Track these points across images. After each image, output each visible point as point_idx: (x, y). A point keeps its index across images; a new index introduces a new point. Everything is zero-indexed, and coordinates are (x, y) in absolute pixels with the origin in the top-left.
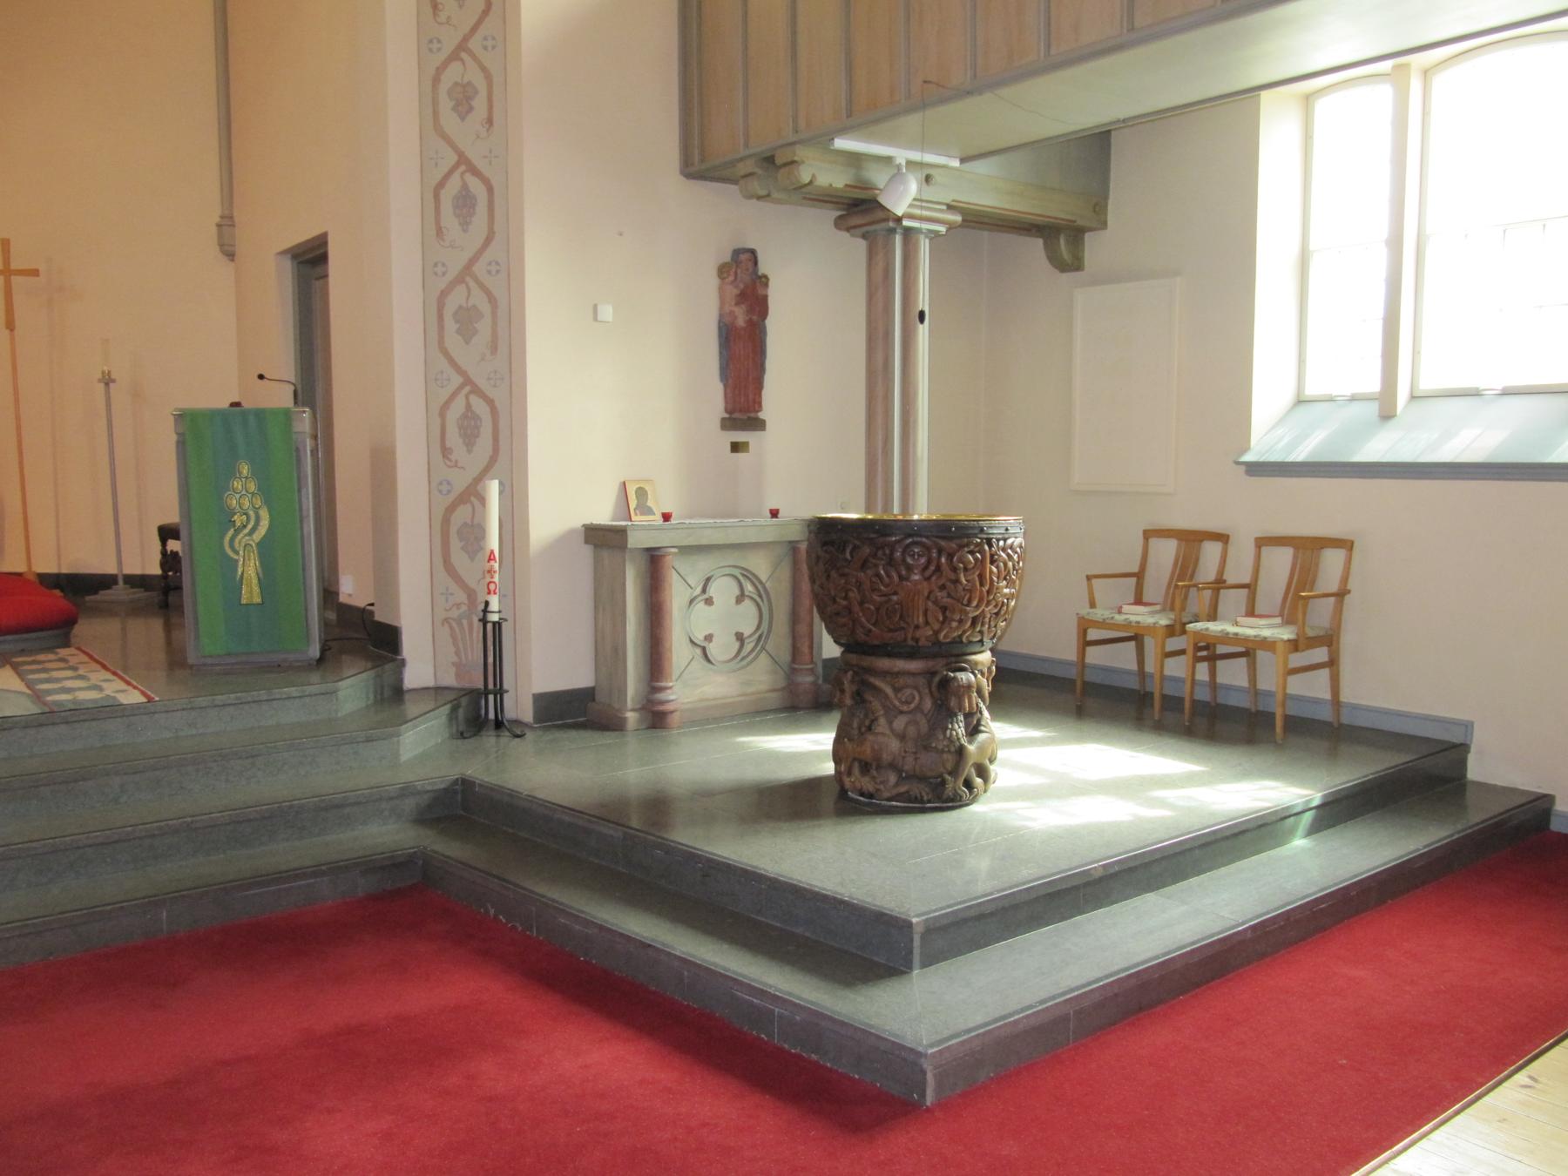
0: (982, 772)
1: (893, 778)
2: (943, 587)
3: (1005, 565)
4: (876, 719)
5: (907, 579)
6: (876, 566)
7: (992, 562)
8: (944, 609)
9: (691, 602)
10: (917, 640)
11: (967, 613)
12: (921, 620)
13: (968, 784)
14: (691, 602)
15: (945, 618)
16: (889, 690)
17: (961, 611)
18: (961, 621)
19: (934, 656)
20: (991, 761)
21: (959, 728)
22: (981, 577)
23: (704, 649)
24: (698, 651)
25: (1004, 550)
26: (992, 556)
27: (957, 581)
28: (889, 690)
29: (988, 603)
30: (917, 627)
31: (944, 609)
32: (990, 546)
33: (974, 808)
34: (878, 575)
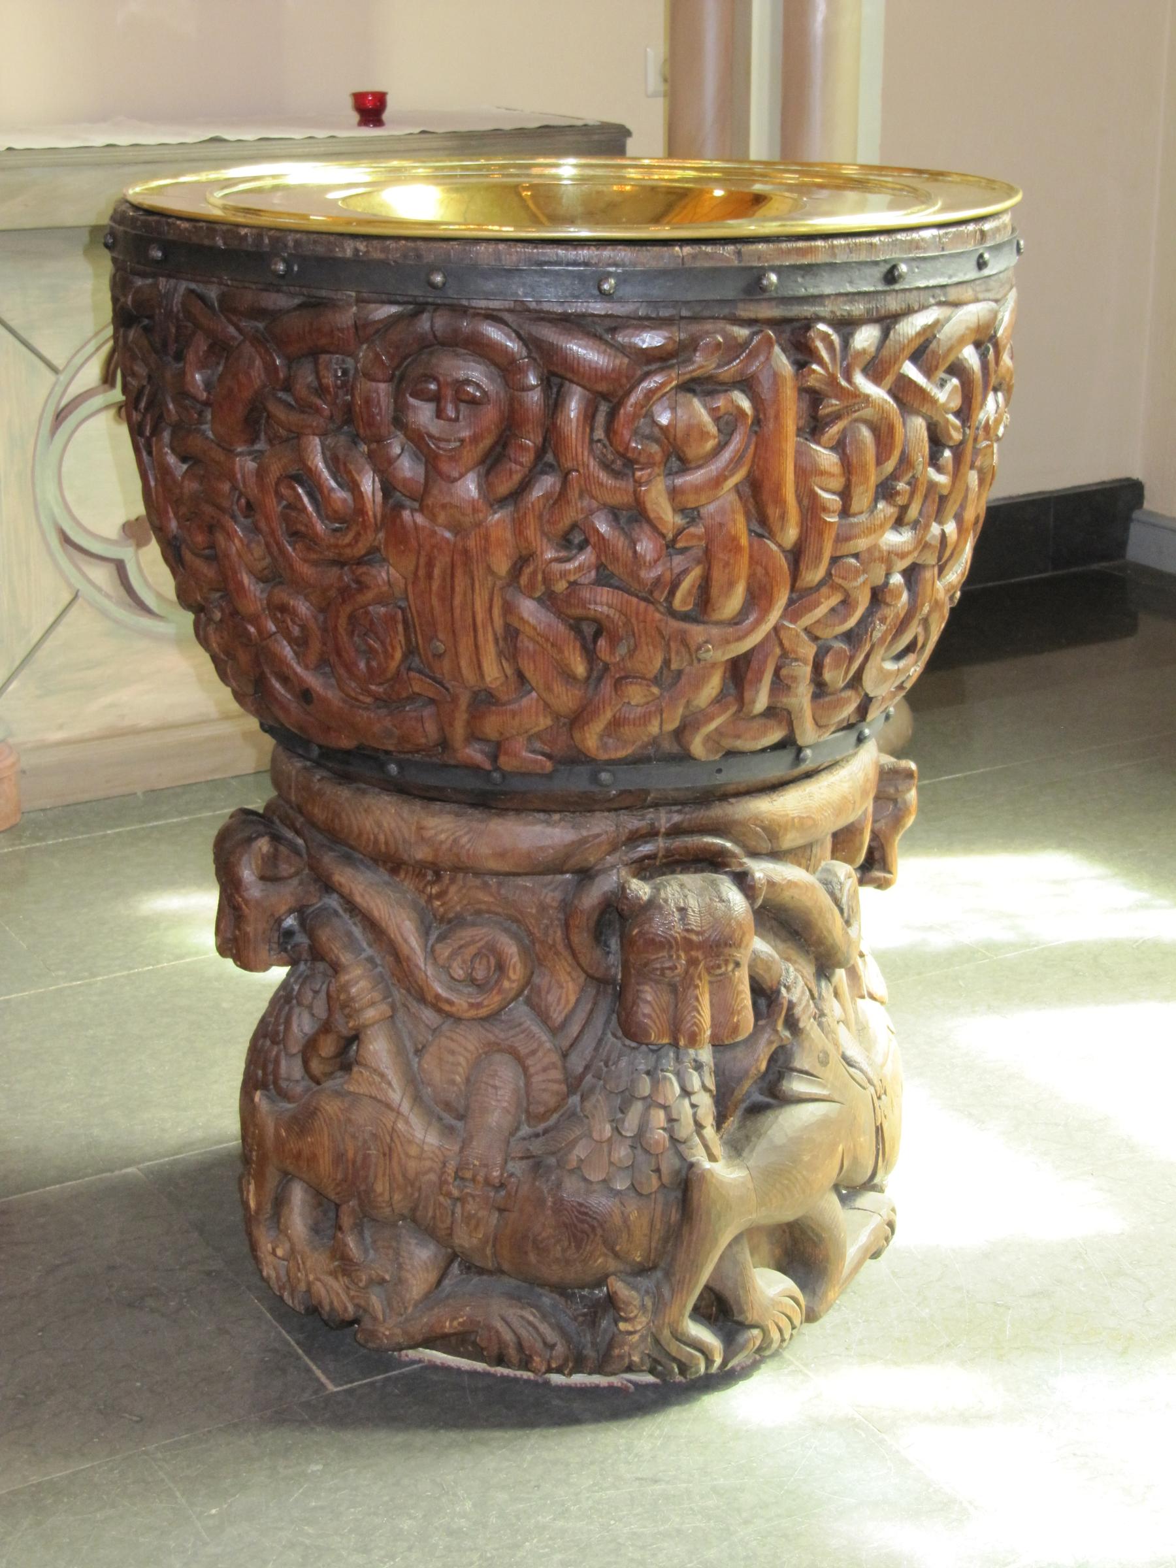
0: (802, 1253)
1: (420, 1259)
2: (572, 539)
3: (883, 434)
4: (355, 1038)
5: (421, 499)
6: (295, 438)
7: (814, 427)
8: (591, 633)
9: (60, 416)
10: (497, 749)
11: (692, 652)
12: (493, 672)
13: (721, 1309)
14: (60, 416)
15: (598, 671)
16: (404, 927)
17: (665, 641)
18: (669, 680)
19: (580, 805)
20: (852, 1188)
21: (688, 1096)
22: (758, 494)
23: (120, 567)
24: (101, 575)
25: (876, 368)
26: (813, 397)
27: (634, 515)
28: (404, 927)
29: (800, 600)
30: (485, 700)
31: (591, 633)
32: (803, 354)
33: (751, 1404)
34: (305, 477)
